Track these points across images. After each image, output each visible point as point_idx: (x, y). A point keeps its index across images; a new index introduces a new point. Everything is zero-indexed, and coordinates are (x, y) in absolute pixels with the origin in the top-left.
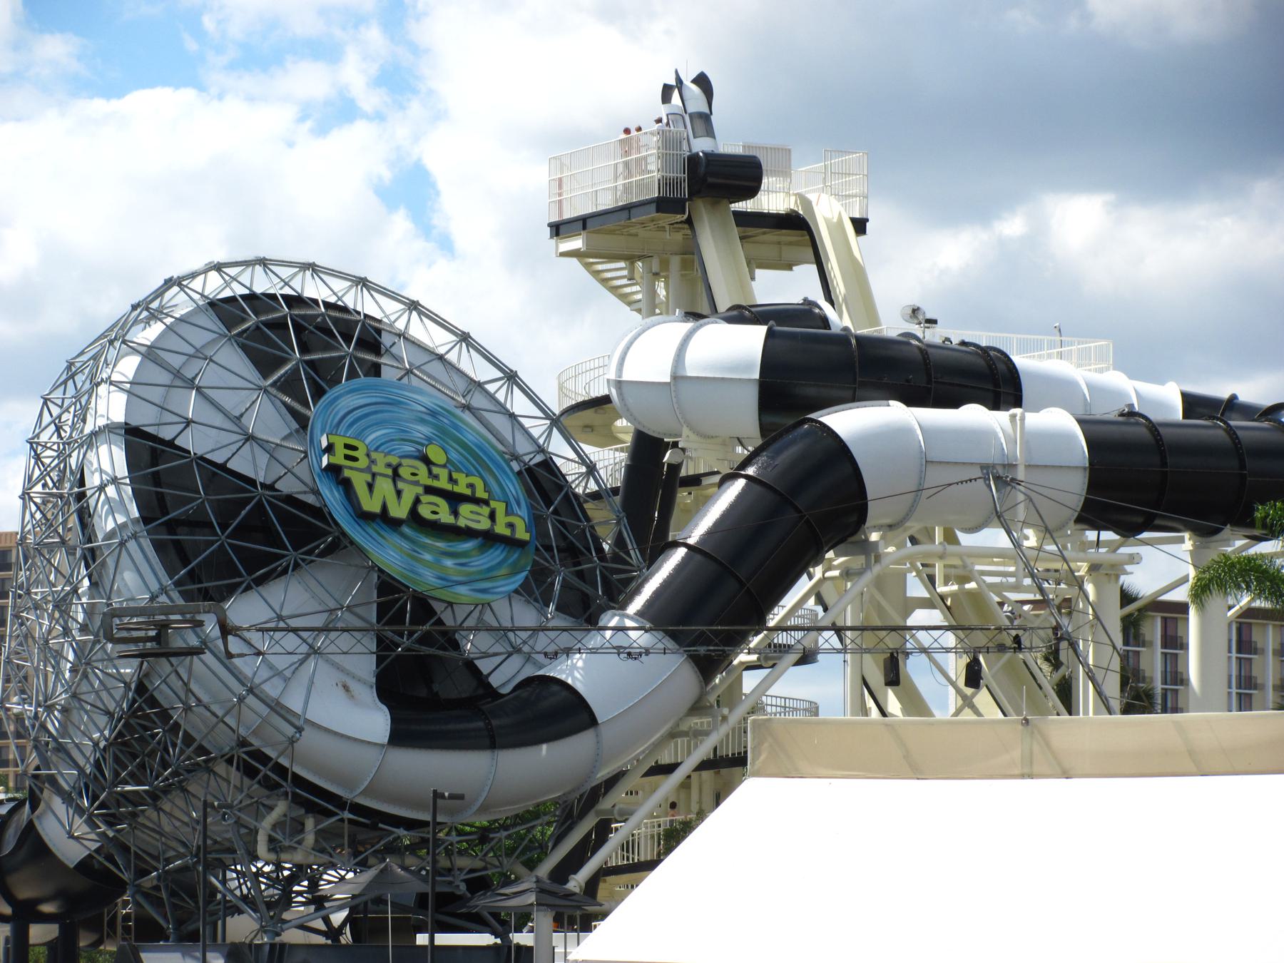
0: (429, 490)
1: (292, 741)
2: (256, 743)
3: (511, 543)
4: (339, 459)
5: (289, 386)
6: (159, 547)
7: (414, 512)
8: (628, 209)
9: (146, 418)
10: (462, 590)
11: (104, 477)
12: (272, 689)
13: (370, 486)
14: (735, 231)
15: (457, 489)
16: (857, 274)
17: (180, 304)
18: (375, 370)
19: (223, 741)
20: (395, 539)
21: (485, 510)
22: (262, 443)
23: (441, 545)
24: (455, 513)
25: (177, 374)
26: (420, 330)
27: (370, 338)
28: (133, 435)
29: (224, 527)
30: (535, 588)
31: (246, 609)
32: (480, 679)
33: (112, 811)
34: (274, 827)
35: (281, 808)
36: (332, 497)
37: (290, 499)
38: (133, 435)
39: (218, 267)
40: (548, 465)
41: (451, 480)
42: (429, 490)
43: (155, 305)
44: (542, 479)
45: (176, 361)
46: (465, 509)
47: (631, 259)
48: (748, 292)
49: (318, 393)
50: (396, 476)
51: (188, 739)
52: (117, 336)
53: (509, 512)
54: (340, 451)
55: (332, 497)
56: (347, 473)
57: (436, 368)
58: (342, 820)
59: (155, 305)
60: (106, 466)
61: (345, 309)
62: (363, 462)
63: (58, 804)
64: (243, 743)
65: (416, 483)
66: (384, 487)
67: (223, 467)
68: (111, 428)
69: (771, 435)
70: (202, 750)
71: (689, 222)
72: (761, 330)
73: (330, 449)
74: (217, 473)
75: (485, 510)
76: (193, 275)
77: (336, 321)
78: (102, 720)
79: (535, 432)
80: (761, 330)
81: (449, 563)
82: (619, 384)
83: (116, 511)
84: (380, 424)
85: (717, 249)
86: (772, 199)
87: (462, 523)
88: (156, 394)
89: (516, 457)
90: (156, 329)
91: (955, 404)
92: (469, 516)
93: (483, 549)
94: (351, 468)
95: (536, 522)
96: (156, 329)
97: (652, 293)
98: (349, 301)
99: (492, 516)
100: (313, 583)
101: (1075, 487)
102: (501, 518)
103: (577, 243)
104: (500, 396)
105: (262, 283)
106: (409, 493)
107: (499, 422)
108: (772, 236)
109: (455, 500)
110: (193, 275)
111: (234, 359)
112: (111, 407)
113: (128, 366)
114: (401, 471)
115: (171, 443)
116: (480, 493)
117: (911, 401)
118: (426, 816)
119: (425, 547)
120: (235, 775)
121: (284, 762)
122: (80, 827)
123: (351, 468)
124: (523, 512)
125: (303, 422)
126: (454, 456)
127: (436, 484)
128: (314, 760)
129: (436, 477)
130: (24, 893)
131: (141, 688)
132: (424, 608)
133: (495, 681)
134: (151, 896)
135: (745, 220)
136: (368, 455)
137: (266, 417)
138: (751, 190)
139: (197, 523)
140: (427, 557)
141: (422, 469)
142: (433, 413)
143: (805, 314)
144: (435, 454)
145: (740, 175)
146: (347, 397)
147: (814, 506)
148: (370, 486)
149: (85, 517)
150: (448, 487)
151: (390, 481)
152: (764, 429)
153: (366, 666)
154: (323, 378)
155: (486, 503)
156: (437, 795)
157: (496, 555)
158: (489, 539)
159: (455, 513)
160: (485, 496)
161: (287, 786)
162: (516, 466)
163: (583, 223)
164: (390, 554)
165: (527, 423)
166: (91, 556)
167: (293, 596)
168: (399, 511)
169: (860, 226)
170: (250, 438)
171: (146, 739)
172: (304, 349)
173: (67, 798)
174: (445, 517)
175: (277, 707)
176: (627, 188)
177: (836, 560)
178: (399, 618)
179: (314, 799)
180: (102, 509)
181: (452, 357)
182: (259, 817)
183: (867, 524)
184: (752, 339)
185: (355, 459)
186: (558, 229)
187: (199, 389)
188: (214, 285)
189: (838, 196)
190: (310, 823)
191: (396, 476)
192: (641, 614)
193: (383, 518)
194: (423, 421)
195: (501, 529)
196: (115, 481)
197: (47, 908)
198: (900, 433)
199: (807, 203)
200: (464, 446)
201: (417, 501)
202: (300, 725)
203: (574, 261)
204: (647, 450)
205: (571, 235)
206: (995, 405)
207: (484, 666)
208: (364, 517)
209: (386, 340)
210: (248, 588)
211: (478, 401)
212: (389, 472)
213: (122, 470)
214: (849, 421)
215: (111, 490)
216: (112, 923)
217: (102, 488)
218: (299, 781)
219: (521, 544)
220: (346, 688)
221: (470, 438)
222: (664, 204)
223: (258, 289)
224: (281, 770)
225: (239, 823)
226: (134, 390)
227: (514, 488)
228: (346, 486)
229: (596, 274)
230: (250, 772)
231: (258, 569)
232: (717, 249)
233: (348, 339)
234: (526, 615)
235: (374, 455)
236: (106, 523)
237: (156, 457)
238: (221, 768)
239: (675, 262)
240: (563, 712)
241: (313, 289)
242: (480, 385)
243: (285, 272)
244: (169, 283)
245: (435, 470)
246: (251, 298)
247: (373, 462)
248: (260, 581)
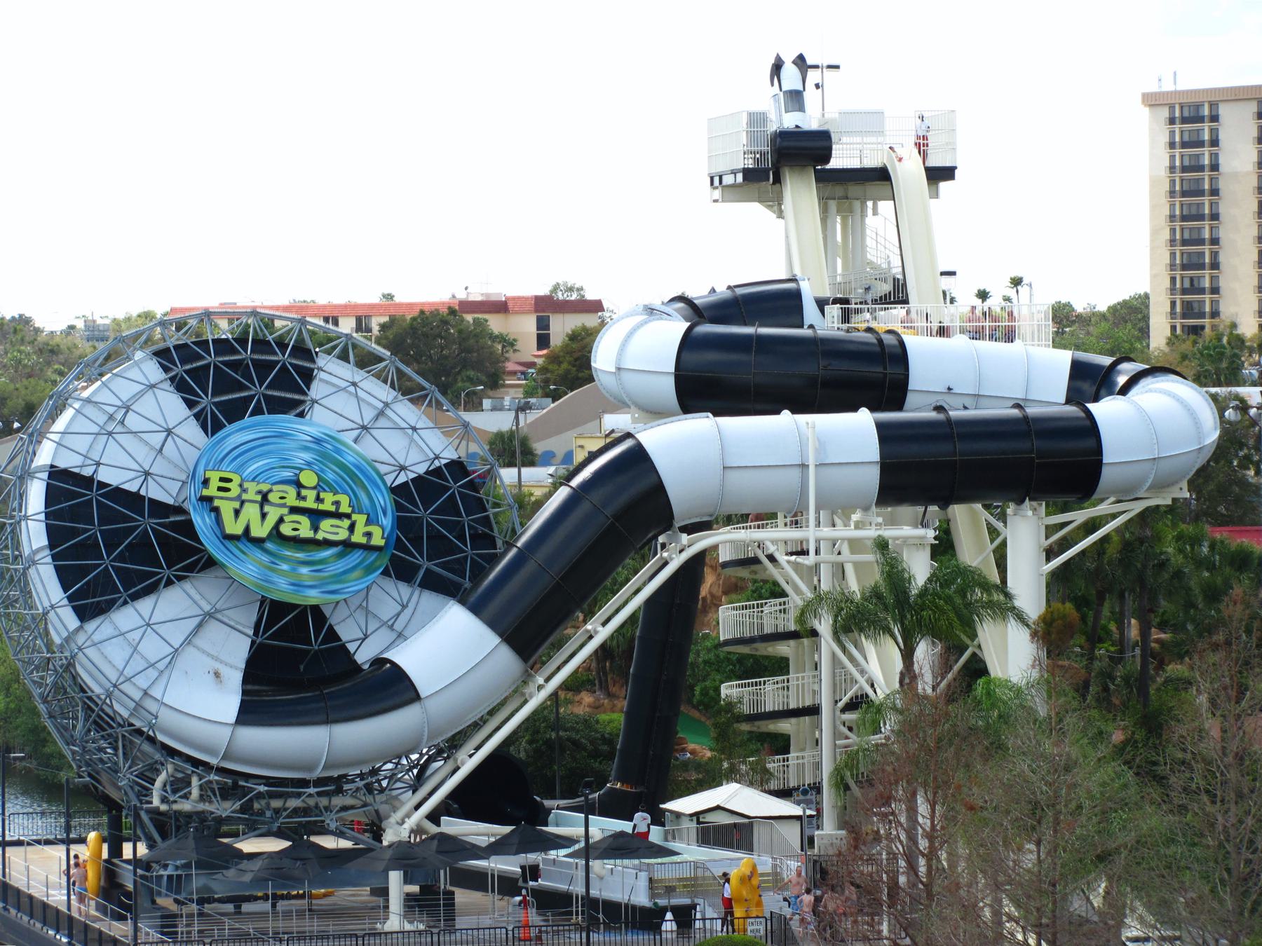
11: (326, 390)
13: (237, 513)
15: (321, 507)
20: (258, 554)
21: (347, 523)
23: (300, 556)
24: (316, 528)
29: (110, 548)
41: (319, 499)
42: (294, 510)
46: (326, 524)
54: (214, 483)
56: (216, 503)
58: (210, 782)
65: (284, 505)
66: (251, 512)
75: (347, 523)
81: (304, 570)
87: (320, 536)
92: (330, 529)
93: (340, 556)
94: (222, 498)
99: (352, 528)
100: (193, 592)
101: (872, 477)
102: (360, 528)
109: (316, 516)
114: (271, 497)
116: (344, 508)
119: (285, 559)
123: (222, 498)
124: (387, 522)
126: (330, 476)
127: (302, 504)
129: (304, 498)
136: (241, 486)
140: (285, 567)
141: (292, 491)
142: (318, 441)
144: (308, 478)
148: (237, 513)
150: (313, 506)
151: (257, 506)
155: (348, 516)
157: (356, 557)
158: (348, 545)
159: (316, 528)
160: (349, 510)
167: (173, 605)
168: (259, 531)
174: (305, 531)
185: (227, 490)
190: (195, 781)
194: (306, 449)
195: (358, 538)
201: (281, 520)
210: (125, 603)
212: (259, 498)
220: (217, 675)
231: (141, 585)
235: (246, 485)
240: (391, 687)
245: (304, 492)
247: (245, 491)
248: (135, 597)
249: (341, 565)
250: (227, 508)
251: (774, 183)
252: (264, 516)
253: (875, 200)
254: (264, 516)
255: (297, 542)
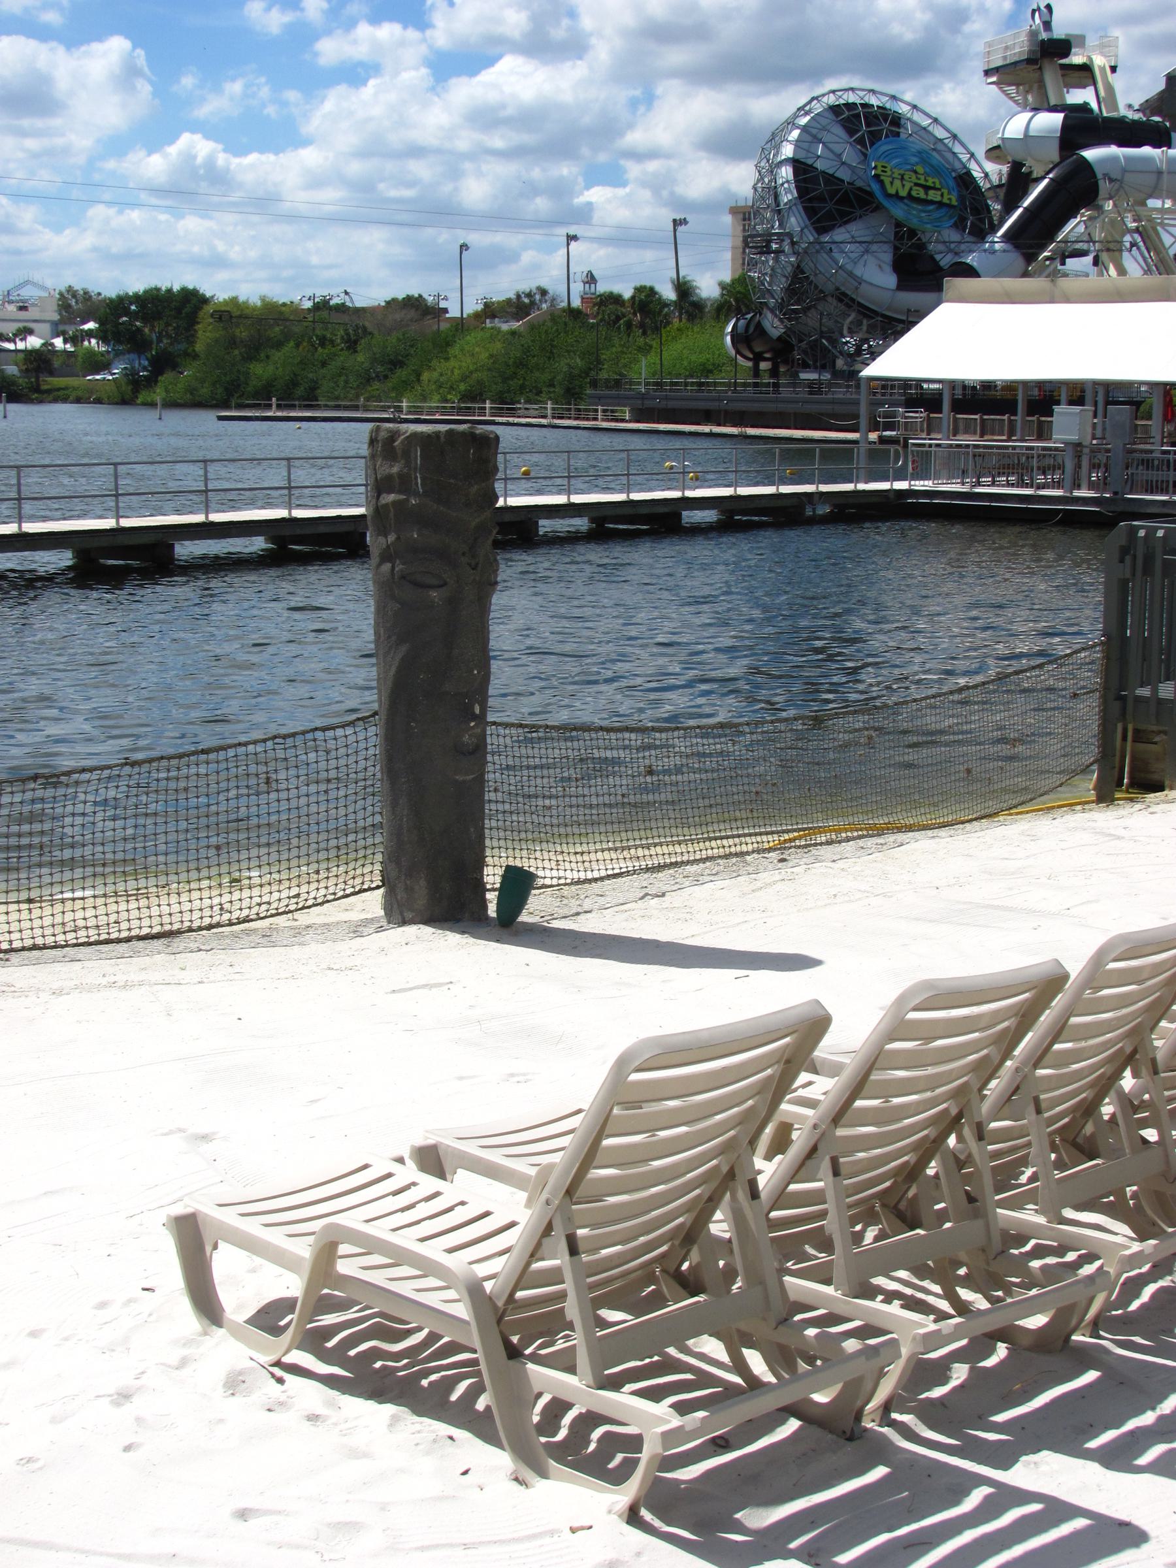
0: (916, 185)
1: (857, 288)
2: (843, 289)
3: (949, 206)
4: (879, 172)
5: (861, 141)
6: (805, 208)
7: (909, 193)
8: (1015, 63)
9: (801, 156)
10: (929, 226)
12: (849, 267)
13: (892, 183)
14: (1060, 72)
16: (1110, 89)
17: (817, 108)
18: (898, 135)
19: (830, 288)
22: (849, 166)
24: (927, 194)
25: (815, 137)
26: (917, 117)
27: (896, 120)
28: (795, 163)
30: (959, 225)
31: (840, 234)
32: (936, 263)
33: (791, 315)
34: (851, 322)
35: (853, 316)
36: (875, 187)
37: (860, 189)
38: (795, 163)
39: (833, 92)
40: (968, 173)
41: (926, 180)
42: (916, 185)
43: (807, 108)
44: (965, 180)
45: (814, 131)
46: (931, 192)
47: (1017, 85)
48: (1063, 98)
49: (872, 144)
50: (902, 179)
51: (816, 287)
52: (790, 123)
53: (949, 193)
54: (880, 169)
55: (875, 187)
57: (922, 133)
59: (807, 108)
60: (784, 175)
61: (885, 109)
62: (889, 173)
63: (769, 315)
64: (838, 289)
66: (898, 183)
67: (832, 176)
68: (787, 160)
69: (1063, 159)
70: (821, 291)
71: (1040, 68)
72: (1061, 116)
73: (875, 168)
74: (830, 179)
76: (824, 95)
77: (882, 114)
78: (784, 280)
79: (964, 160)
80: (1061, 116)
82: (1003, 139)
83: (787, 196)
84: (896, 157)
85: (1051, 78)
86: (1077, 59)
87: (929, 198)
88: (805, 145)
89: (954, 170)
90: (808, 118)
91: (1139, 146)
92: (933, 195)
93: (937, 209)
95: (961, 198)
96: (808, 118)
97: (1026, 99)
98: (888, 106)
99: (942, 195)
103: (994, 79)
104: (950, 145)
105: (852, 98)
106: (908, 186)
107: (949, 156)
108: (1077, 74)
109: (927, 188)
110: (824, 95)
111: (839, 131)
112: (788, 151)
113: (795, 134)
115: (811, 166)
116: (938, 186)
117: (1120, 145)
118: (904, 318)
119: (914, 209)
120: (835, 302)
121: (854, 296)
122: (777, 323)
125: (865, 155)
128: (866, 296)
130: (758, 349)
131: (798, 266)
132: (912, 233)
133: (942, 263)
134: (805, 352)
135: (1065, 67)
137: (849, 154)
138: (1067, 54)
139: (821, 198)
142: (919, 152)
143: (1084, 108)
144: (920, 169)
145: (1063, 47)
146: (884, 146)
147: (1077, 189)
149: (776, 197)
152: (1061, 157)
153: (888, 257)
154: (875, 137)
156: (909, 310)
157: (943, 211)
158: (940, 204)
159: (927, 194)
161: (855, 307)
162: (954, 174)
163: (997, 70)
164: (898, 211)
165: (961, 156)
166: (779, 212)
168: (903, 193)
169: (1114, 69)
170: (843, 163)
171: (800, 285)
172: (868, 125)
173: (772, 311)
174: (922, 195)
175: (851, 274)
176: (1005, 58)
177: (1085, 213)
178: (902, 238)
179: (866, 312)
180: (783, 192)
181: (930, 128)
182: (844, 319)
183: (1100, 197)
184: (1058, 118)
186: (987, 73)
187: (824, 144)
188: (831, 100)
189: (1105, 56)
190: (865, 322)
191: (902, 179)
192: (1003, 236)
193: (897, 196)
195: (945, 201)
196: (788, 182)
197: (767, 355)
198: (1114, 159)
199: (1091, 59)
200: (932, 166)
201: (911, 189)
202: (860, 281)
203: (994, 87)
204: (1016, 167)
205: (992, 75)
206: (1156, 145)
207: (938, 257)
208: (889, 196)
209: (903, 122)
211: (940, 147)
213: (791, 177)
214: (1090, 154)
215: (786, 185)
216: (793, 361)
217: (782, 185)
218: (860, 304)
219: (954, 207)
221: (934, 162)
222: (1030, 61)
223: (850, 101)
224: (853, 300)
225: (836, 321)
226: (798, 144)
227: (951, 183)
228: (882, 183)
229: (1004, 92)
230: (841, 301)
232: (1051, 78)
233: (886, 121)
234: (955, 236)
236: (785, 198)
237: (805, 172)
238: (830, 299)
239: (1035, 86)
241: (874, 101)
242: (941, 140)
243: (861, 94)
244: (813, 99)
246: (847, 105)
249: (937, 215)
250: (887, 181)
251: (569, 1406)
252: (903, 186)
253: (377, 664)
254: (903, 186)
255: (918, 200)
